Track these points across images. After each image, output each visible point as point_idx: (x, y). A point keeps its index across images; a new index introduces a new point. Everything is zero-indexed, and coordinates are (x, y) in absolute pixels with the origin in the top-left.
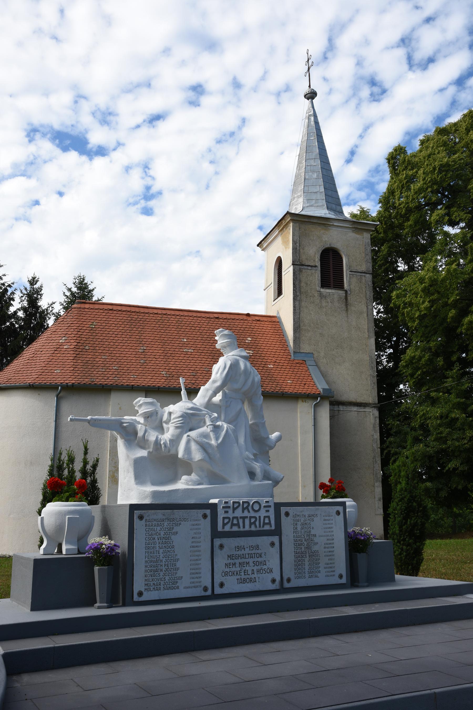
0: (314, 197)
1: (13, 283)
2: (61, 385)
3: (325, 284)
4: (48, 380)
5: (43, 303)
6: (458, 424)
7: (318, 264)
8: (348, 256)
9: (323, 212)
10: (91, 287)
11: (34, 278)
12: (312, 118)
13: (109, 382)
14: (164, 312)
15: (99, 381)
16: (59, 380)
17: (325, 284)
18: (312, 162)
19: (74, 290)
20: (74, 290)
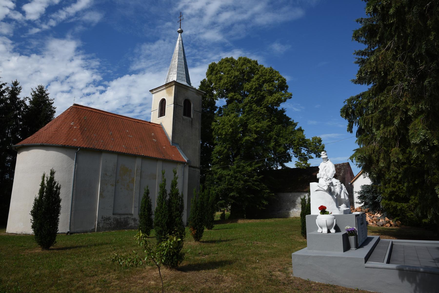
0: (181, 76)
1: (6, 83)
2: (80, 147)
3: (184, 115)
4: (69, 143)
5: (21, 96)
6: (238, 179)
7: (183, 105)
8: (193, 104)
9: (185, 83)
10: (47, 92)
11: (16, 82)
12: (181, 42)
13: (102, 148)
14: (115, 116)
15: (97, 147)
16: (78, 145)
17: (184, 115)
18: (181, 60)
19: (37, 93)
20: (37, 93)
